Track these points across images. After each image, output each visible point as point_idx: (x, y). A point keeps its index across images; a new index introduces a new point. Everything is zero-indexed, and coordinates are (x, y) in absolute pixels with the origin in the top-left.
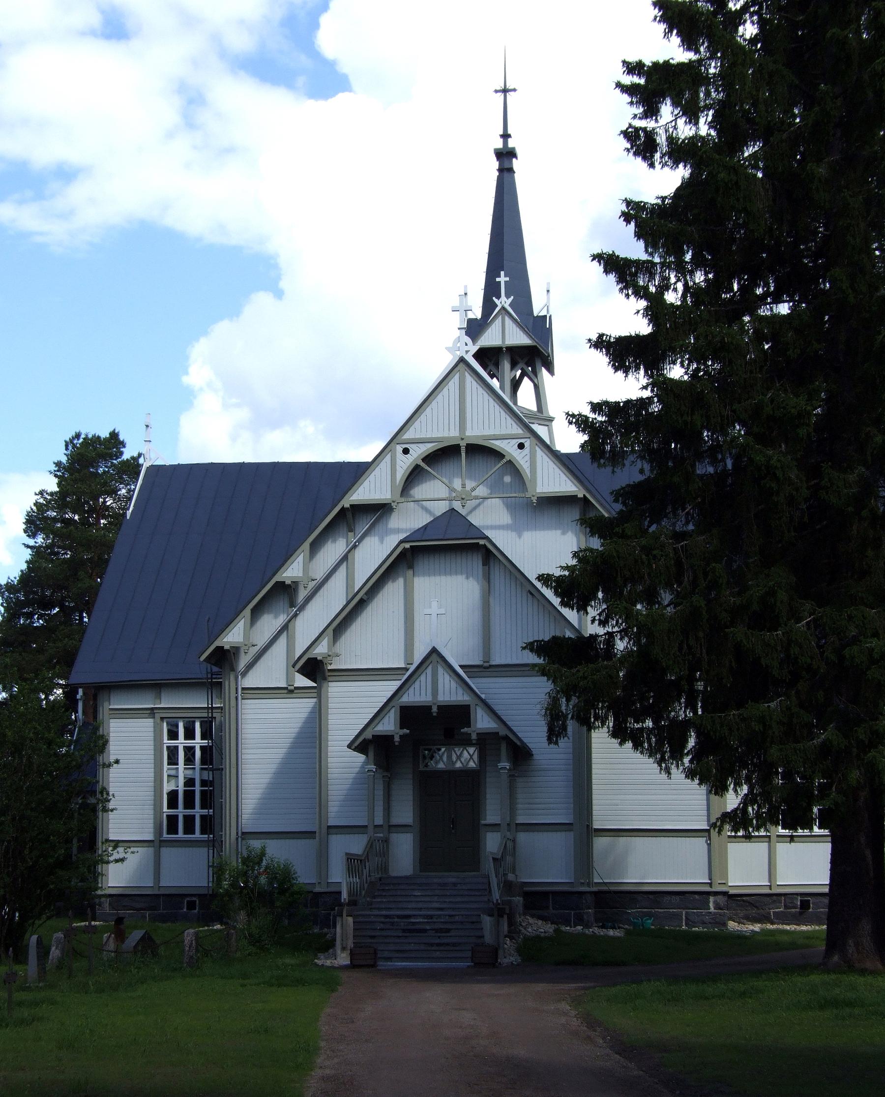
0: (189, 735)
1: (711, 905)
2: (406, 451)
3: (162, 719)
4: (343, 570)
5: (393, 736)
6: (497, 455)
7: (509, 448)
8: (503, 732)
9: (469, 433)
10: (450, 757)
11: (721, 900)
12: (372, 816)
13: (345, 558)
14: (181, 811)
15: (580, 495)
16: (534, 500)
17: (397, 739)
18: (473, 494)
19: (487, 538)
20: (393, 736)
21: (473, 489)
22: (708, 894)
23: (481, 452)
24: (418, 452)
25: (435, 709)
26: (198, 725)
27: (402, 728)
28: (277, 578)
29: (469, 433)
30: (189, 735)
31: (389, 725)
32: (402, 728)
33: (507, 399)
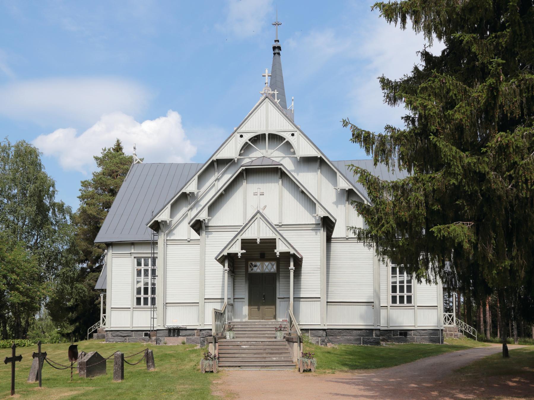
0: (146, 265)
1: (374, 335)
3: (135, 257)
5: (237, 254)
7: (287, 136)
8: (292, 252)
9: (269, 129)
10: (263, 267)
11: (378, 332)
14: (398, 294)
15: (319, 156)
16: (298, 158)
17: (239, 255)
19: (281, 165)
20: (237, 254)
22: (372, 330)
23: (275, 138)
24: (247, 138)
25: (258, 241)
26: (150, 260)
27: (242, 249)
28: (184, 191)
29: (269, 129)
30: (146, 265)
31: (237, 249)
32: (242, 249)
33: (241, 228)
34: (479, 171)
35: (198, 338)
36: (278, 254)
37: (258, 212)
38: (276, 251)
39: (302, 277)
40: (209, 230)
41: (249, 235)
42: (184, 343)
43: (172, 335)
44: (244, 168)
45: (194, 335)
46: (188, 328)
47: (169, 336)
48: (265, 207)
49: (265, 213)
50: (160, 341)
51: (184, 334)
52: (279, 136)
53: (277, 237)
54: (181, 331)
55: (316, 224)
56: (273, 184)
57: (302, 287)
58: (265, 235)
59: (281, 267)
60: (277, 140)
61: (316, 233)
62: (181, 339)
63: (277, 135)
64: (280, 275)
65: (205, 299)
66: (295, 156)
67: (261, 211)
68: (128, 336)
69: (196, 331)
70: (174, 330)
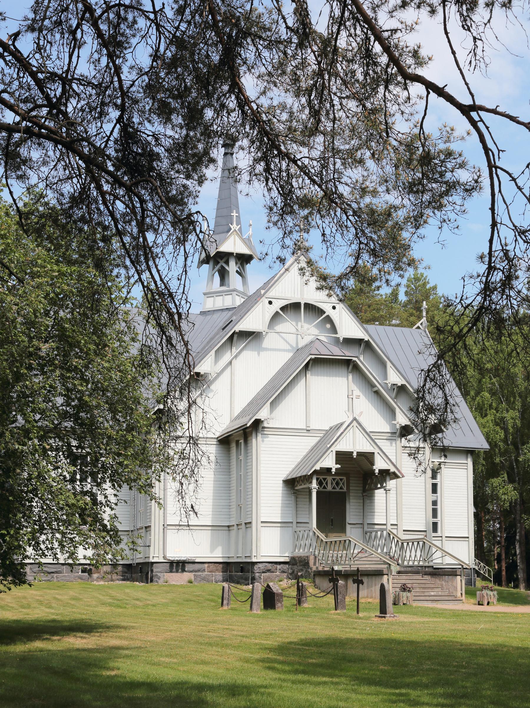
2: (270, 303)
4: (229, 368)
5: (331, 469)
6: (322, 312)
9: (305, 297)
12: (237, 551)
13: (230, 363)
16: (341, 339)
17: (333, 470)
18: (308, 332)
20: (331, 469)
21: (308, 329)
24: (277, 305)
25: (355, 454)
27: (336, 464)
32: (336, 464)
34: (69, 202)
35: (209, 575)
36: (377, 471)
37: (355, 419)
38: (374, 467)
39: (376, 498)
40: (265, 432)
41: (344, 446)
42: (190, 582)
43: (174, 570)
44: (313, 357)
45: (204, 570)
46: (198, 560)
47: (171, 572)
48: (362, 413)
49: (361, 420)
50: (159, 579)
51: (191, 570)
52: (318, 308)
53: (376, 451)
54: (186, 565)
55: (392, 433)
56: (341, 378)
57: (376, 510)
58: (361, 448)
59: (351, 485)
60: (309, 311)
61: (391, 443)
62: (187, 576)
63: (315, 306)
64: (351, 494)
65: (404, 531)
66: (337, 336)
67: (357, 418)
68: (56, 572)
69: (206, 565)
70: (178, 563)
